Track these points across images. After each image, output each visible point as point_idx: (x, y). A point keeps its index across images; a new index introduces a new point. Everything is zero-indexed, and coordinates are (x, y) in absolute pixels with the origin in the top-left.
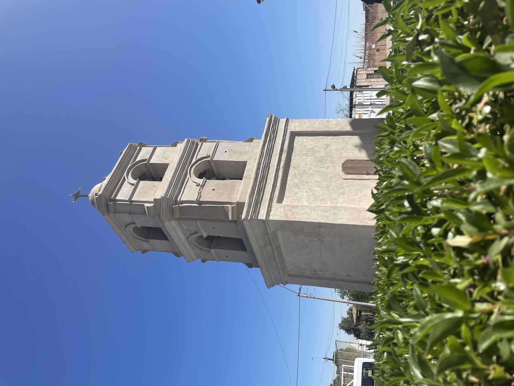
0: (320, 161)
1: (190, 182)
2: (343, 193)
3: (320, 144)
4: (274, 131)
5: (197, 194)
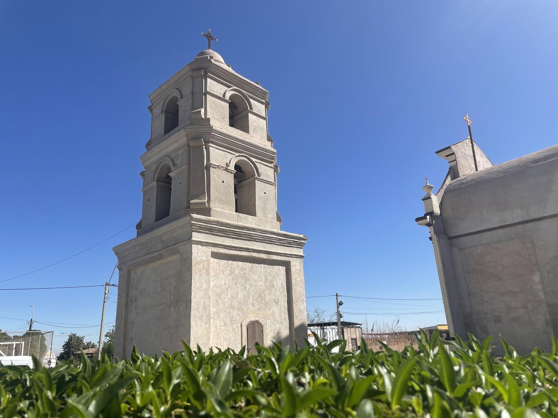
0: (260, 296)
1: (230, 156)
2: (225, 324)
3: (278, 294)
4: (290, 243)
5: (217, 164)
